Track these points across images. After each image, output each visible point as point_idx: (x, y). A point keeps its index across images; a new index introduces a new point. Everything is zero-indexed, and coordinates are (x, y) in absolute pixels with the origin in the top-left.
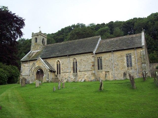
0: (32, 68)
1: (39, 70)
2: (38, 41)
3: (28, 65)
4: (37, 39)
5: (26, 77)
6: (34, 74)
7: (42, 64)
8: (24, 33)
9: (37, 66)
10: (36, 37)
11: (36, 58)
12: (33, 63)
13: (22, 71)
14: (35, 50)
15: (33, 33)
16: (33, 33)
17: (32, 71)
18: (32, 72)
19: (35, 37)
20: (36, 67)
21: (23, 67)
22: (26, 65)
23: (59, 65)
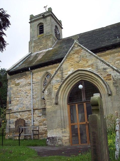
0: (15, 112)
1: (81, 86)
2: (46, 29)
3: (29, 80)
4: (43, 26)
5: (25, 116)
6: (61, 102)
7: (90, 63)
8: (7, 43)
9: (70, 73)
10: (41, 21)
11: (59, 57)
12: (43, 73)
13: (10, 98)
14: (41, 49)
15: (32, 17)
16: (32, 17)
17: (50, 93)
18: (53, 96)
19: (37, 23)
20: (64, 78)
21: (15, 89)
22: (22, 81)
23: (64, 101)
